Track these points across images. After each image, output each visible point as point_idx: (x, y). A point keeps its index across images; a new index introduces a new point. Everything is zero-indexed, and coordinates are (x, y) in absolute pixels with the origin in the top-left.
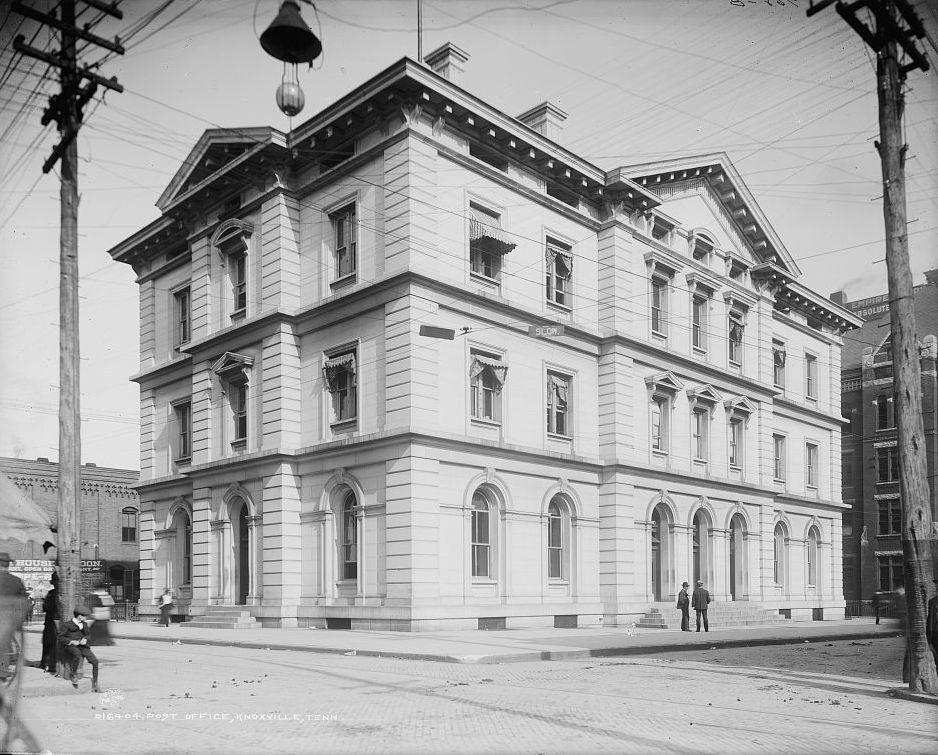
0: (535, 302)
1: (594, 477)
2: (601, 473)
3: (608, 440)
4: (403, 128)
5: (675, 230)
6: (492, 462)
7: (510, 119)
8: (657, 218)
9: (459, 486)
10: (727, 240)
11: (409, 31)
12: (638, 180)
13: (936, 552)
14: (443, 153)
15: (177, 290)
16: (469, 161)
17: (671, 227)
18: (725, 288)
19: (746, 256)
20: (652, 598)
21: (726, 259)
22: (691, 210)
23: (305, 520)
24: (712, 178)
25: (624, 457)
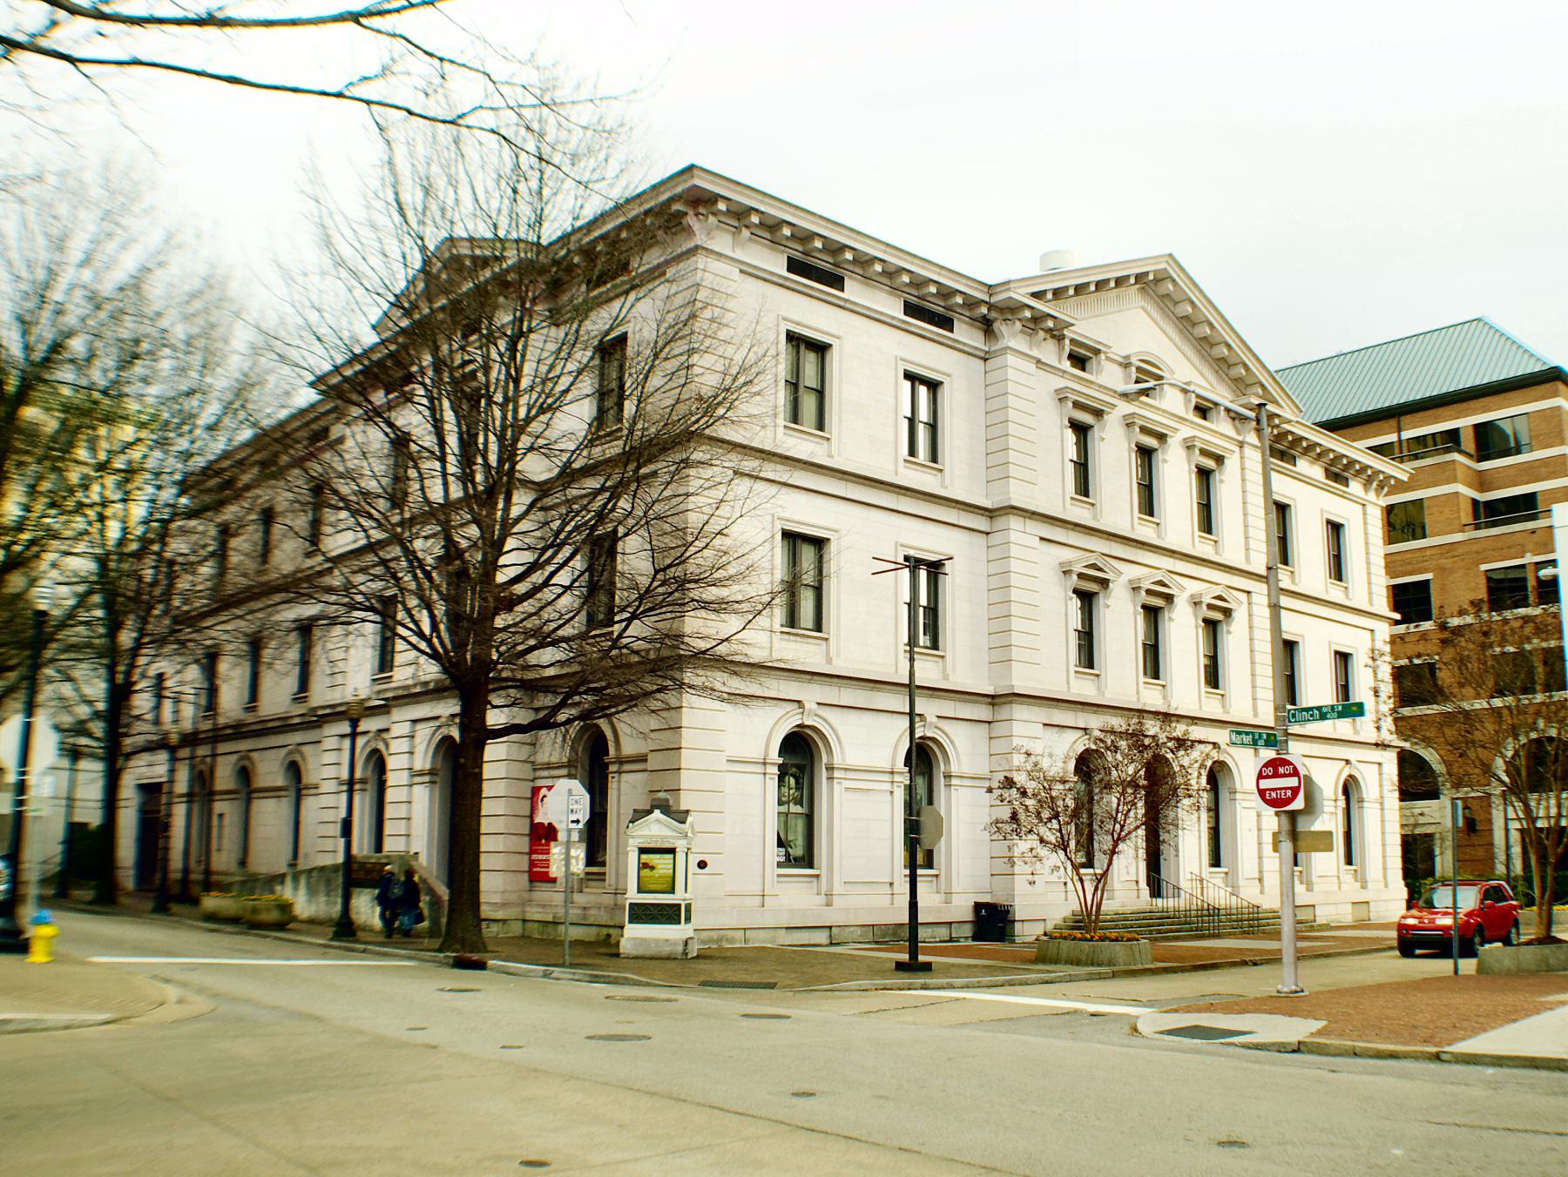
0: (888, 461)
1: (982, 712)
2: (993, 705)
3: (1001, 653)
4: (691, 244)
5: (1103, 356)
6: (811, 694)
7: (1269, 372)
8: (1072, 341)
9: (758, 732)
10: (1184, 368)
11: (397, 11)
12: (1037, 295)
13: (161, 843)
14: (749, 272)
15: (912, 553)
16: (786, 279)
17: (1097, 352)
18: (1186, 432)
19: (1221, 394)
20: (1145, 890)
21: (1185, 391)
22: (1129, 330)
23: (417, 779)
24: (1156, 285)
25: (1021, 682)
